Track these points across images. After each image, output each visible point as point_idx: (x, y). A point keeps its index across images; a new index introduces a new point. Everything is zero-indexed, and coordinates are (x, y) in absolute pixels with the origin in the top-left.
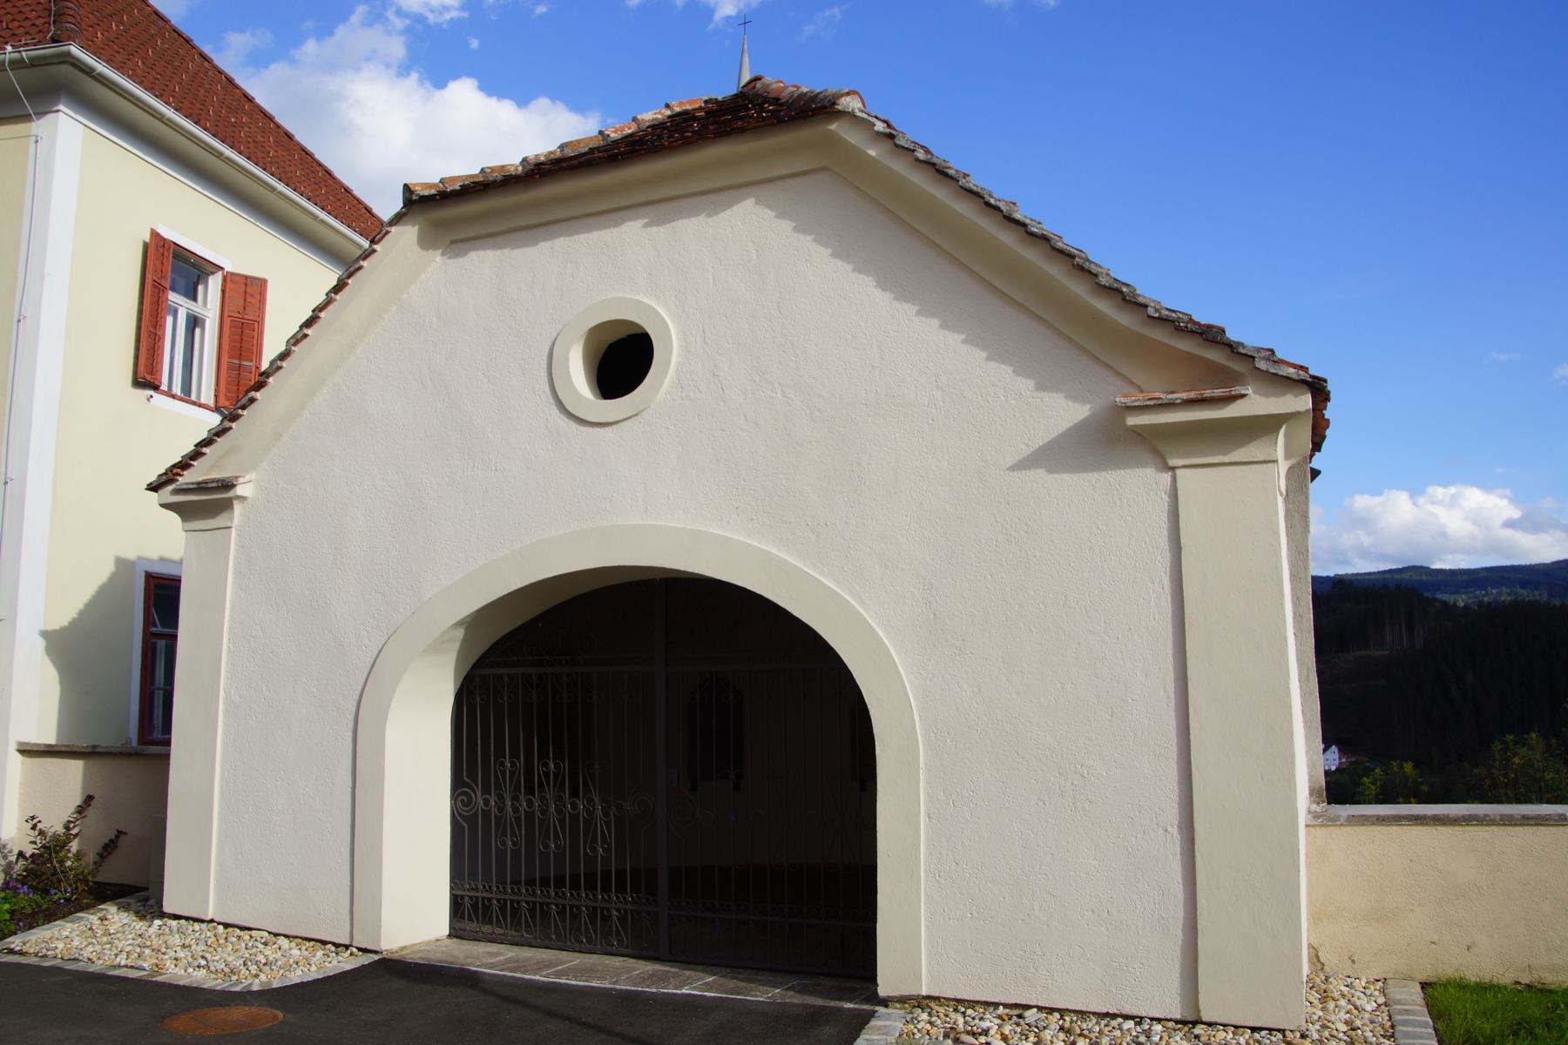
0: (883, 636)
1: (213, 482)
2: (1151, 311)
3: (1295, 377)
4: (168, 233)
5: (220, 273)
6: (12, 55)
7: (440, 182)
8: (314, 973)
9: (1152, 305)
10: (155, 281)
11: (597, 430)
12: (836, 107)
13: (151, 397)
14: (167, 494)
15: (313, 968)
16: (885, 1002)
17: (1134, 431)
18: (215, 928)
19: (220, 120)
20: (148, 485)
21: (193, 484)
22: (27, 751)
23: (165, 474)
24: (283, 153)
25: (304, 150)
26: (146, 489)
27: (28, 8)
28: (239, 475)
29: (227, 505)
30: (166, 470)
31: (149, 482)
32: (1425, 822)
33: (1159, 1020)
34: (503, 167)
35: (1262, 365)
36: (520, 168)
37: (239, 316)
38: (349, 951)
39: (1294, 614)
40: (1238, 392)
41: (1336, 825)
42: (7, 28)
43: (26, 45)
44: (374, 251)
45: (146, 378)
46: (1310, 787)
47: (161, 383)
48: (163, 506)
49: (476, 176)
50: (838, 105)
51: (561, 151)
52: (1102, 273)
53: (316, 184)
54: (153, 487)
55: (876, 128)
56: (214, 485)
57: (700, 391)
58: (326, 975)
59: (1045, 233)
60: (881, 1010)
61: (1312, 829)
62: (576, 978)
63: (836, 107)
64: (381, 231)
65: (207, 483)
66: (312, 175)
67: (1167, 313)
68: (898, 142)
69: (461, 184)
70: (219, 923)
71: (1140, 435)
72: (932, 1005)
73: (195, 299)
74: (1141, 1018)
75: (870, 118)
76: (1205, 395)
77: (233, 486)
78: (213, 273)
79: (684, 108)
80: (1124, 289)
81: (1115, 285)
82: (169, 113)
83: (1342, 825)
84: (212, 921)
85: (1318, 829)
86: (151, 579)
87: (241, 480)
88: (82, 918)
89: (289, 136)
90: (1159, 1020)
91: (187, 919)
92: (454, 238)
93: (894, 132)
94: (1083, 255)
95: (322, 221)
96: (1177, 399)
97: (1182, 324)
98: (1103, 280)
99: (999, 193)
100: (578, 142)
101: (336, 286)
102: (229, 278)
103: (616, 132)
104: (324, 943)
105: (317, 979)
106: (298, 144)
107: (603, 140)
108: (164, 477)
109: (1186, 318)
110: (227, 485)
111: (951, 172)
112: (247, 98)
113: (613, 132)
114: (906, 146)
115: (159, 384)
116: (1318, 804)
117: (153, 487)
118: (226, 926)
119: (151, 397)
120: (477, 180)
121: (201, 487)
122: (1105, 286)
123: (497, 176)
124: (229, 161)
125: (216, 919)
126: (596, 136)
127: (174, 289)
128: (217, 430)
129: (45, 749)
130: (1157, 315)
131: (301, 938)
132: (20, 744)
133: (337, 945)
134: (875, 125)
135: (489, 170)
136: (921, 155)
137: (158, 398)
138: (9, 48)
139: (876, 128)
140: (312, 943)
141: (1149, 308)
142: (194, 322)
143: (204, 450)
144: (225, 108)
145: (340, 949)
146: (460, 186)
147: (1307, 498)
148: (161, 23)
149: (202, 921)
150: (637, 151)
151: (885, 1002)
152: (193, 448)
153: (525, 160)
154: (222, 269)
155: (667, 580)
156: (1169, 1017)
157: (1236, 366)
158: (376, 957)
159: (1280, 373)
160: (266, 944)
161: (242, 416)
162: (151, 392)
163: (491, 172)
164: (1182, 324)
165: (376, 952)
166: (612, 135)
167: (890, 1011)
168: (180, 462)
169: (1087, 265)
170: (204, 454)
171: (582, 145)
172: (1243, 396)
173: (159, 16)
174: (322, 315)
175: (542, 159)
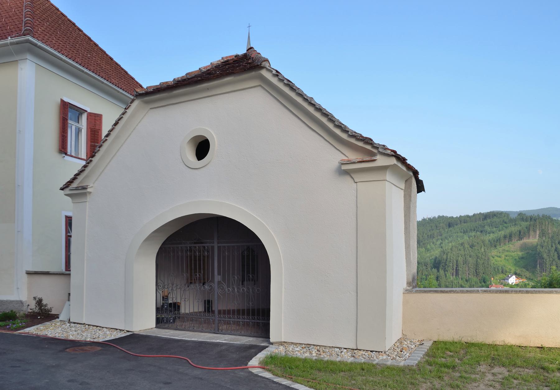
0: (273, 234)
1: (80, 187)
2: (350, 133)
3: (390, 154)
4: (66, 100)
5: (86, 113)
6: (11, 40)
7: (146, 88)
8: (113, 337)
9: (350, 131)
10: (63, 117)
11: (194, 170)
12: (261, 65)
13: (64, 157)
14: (67, 191)
15: (112, 336)
16: (272, 344)
17: (345, 171)
18: (85, 326)
19: (84, 57)
20: (61, 188)
21: (74, 188)
22: (29, 273)
23: (65, 185)
24: (108, 67)
25: (117, 64)
26: (60, 190)
27: (17, 20)
28: (88, 185)
29: (85, 194)
30: (66, 183)
31: (60, 187)
32: (438, 292)
33: (346, 349)
34: (167, 82)
35: (381, 150)
36: (172, 83)
37: (93, 128)
38: (124, 332)
39: (405, 227)
40: (373, 159)
41: (412, 293)
42: (10, 29)
43: (15, 36)
44: (126, 112)
45: (63, 149)
46: (407, 282)
47: (67, 152)
48: (66, 195)
49: (158, 85)
50: (262, 65)
51: (186, 76)
52: (336, 121)
53: (120, 78)
54: (62, 189)
55: (273, 73)
56: (80, 188)
57: (223, 158)
58: (116, 338)
59: (320, 108)
60: (271, 346)
61: (405, 294)
62: (188, 338)
63: (261, 65)
64: (128, 105)
65: (78, 188)
66: (119, 74)
67: (354, 133)
68: (279, 77)
69: (153, 89)
70: (87, 325)
71: (347, 172)
72: (285, 345)
73: (78, 123)
74: (341, 348)
75: (271, 69)
76: (364, 160)
77: (86, 189)
78: (83, 113)
79: (228, 59)
80: (342, 126)
81: (340, 125)
82: (64, 58)
83: (413, 293)
84: (84, 324)
85: (407, 294)
86: (67, 218)
87: (89, 187)
88: (47, 324)
89: (112, 59)
90: (346, 349)
91: (77, 323)
92: (150, 108)
93: (278, 74)
94: (331, 115)
95: (121, 93)
96: (356, 161)
97: (358, 137)
98: (336, 123)
99: (309, 93)
100: (192, 72)
101: (115, 123)
102: (90, 115)
103: (204, 69)
104: (117, 329)
105: (113, 339)
106: (115, 62)
107: (200, 72)
108: (65, 186)
109: (360, 135)
110: (84, 188)
111: (294, 88)
112: (96, 45)
113: (203, 68)
114: (281, 79)
115: (66, 152)
116: (409, 287)
117: (62, 189)
118: (89, 325)
119: (64, 157)
120: (158, 87)
121: (77, 189)
122: (337, 125)
123: (165, 85)
124: (86, 73)
125: (86, 323)
126: (198, 70)
127: (71, 119)
128: (80, 170)
129: (34, 273)
130: (351, 134)
131: (110, 328)
132: (27, 271)
133: (120, 330)
134: (272, 71)
135: (162, 84)
136: (286, 82)
137: (67, 158)
138: (9, 38)
139: (273, 73)
140: (113, 330)
141: (349, 132)
142: (79, 131)
143: (77, 177)
144: (86, 51)
145: (121, 331)
146: (153, 90)
147: (411, 190)
148: (63, 18)
149: (82, 324)
150: (203, 80)
151: (272, 344)
152: (73, 176)
153: (174, 79)
154: (86, 111)
155: (218, 217)
156: (349, 348)
157: (375, 151)
158: (132, 333)
159: (386, 153)
160: (100, 330)
161: (88, 166)
162: (64, 155)
163: (163, 84)
164: (358, 137)
165: (132, 332)
166: (203, 70)
167: (273, 346)
168: (70, 181)
169: (332, 118)
170: (77, 178)
171: (193, 74)
172: (375, 160)
173: (63, 15)
174: (111, 133)
175: (180, 79)
